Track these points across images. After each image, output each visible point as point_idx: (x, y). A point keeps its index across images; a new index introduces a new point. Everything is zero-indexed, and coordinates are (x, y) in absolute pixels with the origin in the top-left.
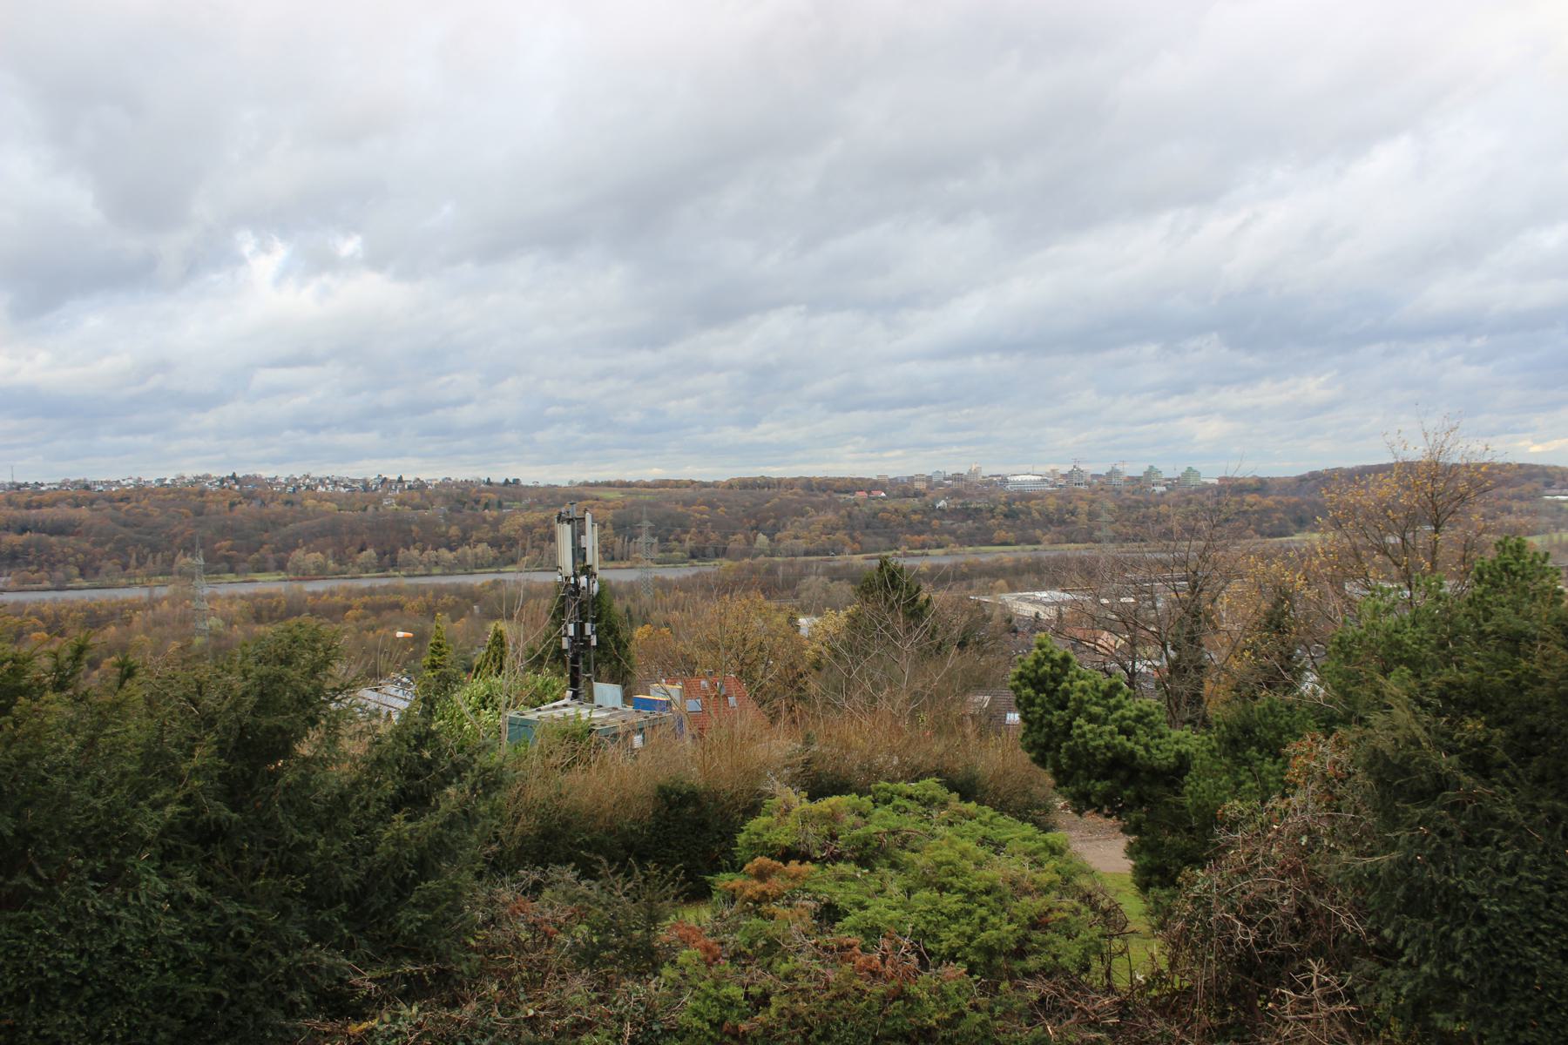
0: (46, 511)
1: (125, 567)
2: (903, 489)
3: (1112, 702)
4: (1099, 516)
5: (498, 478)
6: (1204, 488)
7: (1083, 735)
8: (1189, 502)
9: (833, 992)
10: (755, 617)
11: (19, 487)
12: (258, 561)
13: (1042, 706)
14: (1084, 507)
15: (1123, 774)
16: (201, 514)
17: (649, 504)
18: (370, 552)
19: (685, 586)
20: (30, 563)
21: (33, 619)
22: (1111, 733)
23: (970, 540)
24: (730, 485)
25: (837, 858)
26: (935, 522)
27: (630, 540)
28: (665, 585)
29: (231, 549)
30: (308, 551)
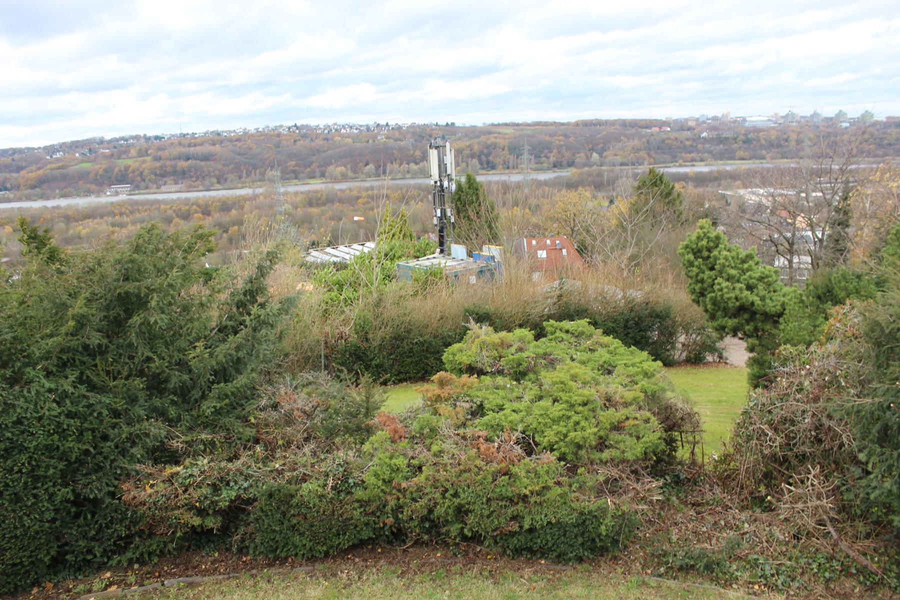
0: (198, 148)
1: (240, 177)
2: (681, 126)
3: (746, 266)
4: (803, 142)
5: (442, 122)
6: (875, 124)
7: (721, 290)
8: (864, 133)
9: (462, 467)
10: (585, 201)
11: (184, 135)
12: (310, 173)
13: (699, 267)
14: (794, 136)
15: (746, 316)
16: (279, 147)
17: (529, 136)
18: (371, 167)
19: (546, 183)
20: (192, 177)
21: (195, 207)
22: (741, 289)
23: (721, 156)
24: (577, 124)
25: (500, 372)
26: (700, 146)
27: (517, 157)
28: (539, 184)
29: (296, 166)
30: (337, 166)
